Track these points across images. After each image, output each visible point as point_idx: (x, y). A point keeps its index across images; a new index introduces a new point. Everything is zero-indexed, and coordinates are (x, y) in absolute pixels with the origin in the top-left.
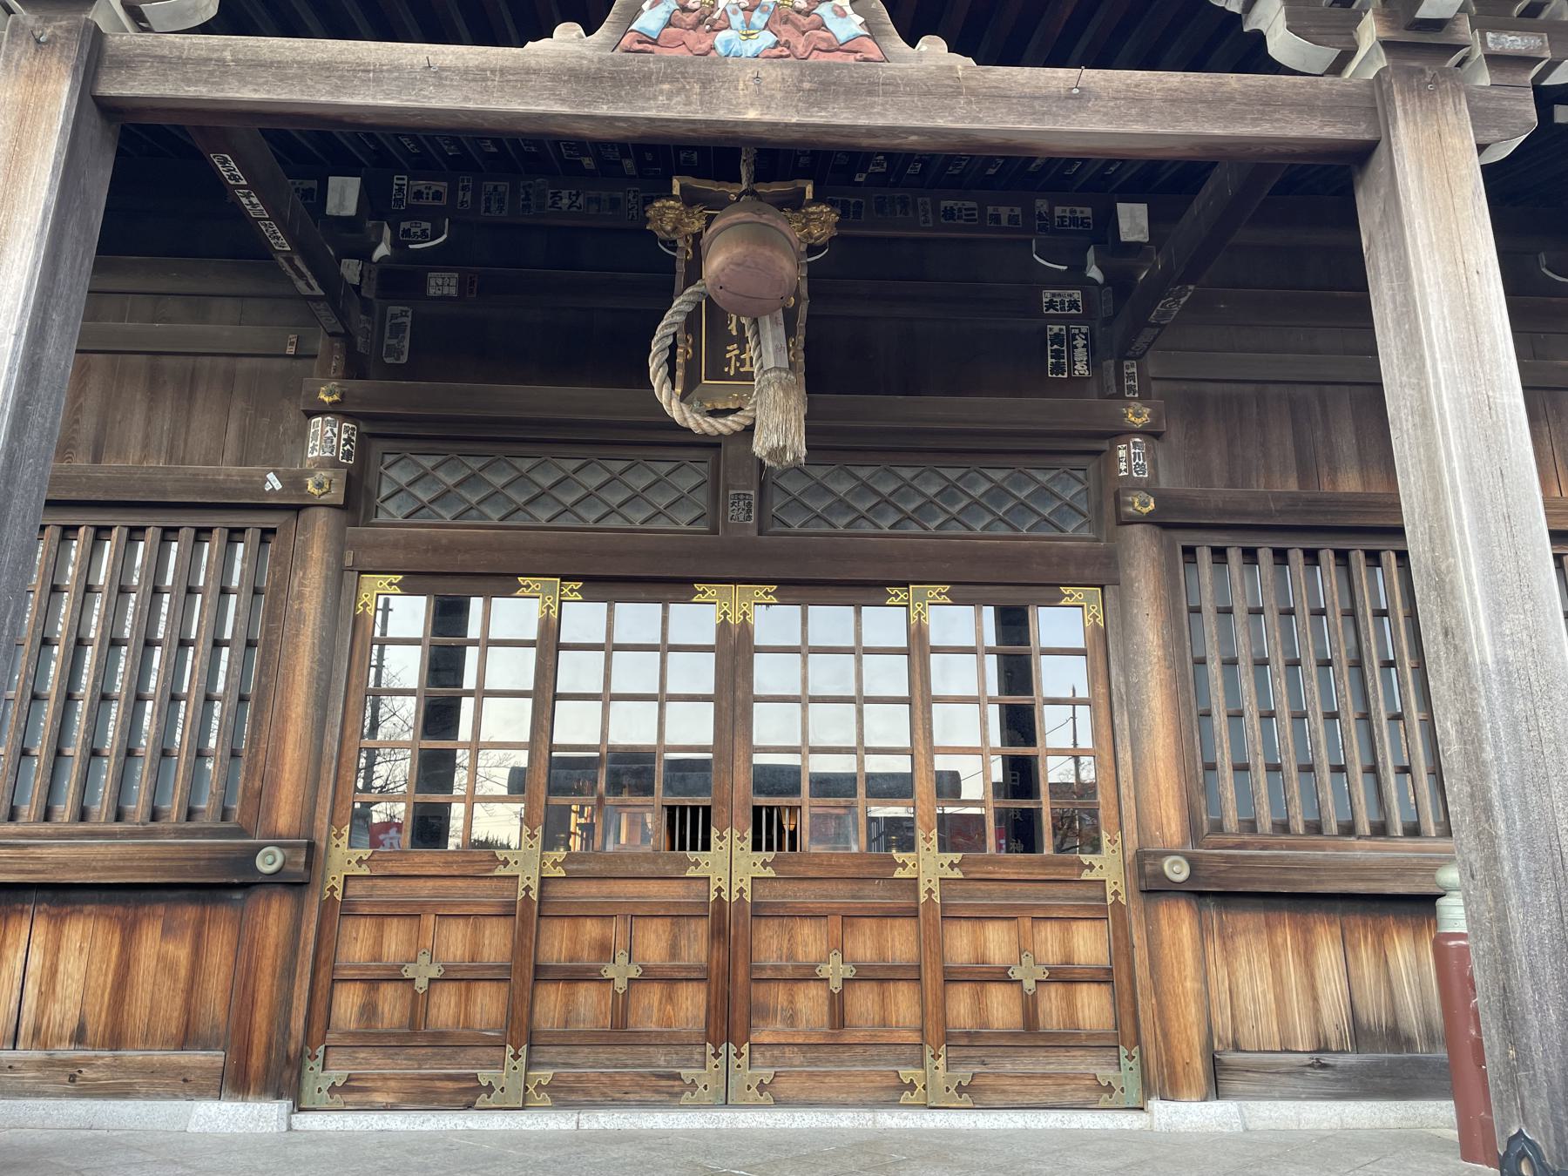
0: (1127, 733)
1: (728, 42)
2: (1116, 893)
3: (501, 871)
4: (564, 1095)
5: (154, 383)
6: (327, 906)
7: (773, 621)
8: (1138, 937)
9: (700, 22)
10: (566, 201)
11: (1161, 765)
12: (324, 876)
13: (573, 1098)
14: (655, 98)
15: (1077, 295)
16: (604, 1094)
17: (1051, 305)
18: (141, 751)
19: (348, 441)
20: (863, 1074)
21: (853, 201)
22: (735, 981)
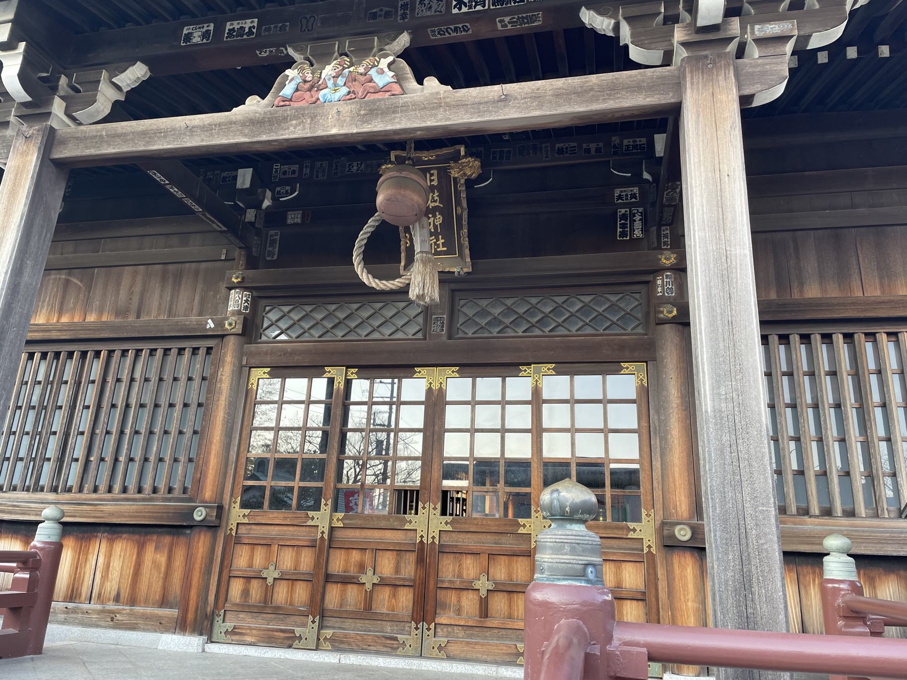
0: (658, 450)
1: (324, 95)
2: (649, 547)
3: (310, 523)
4: (339, 645)
5: (164, 278)
6: (228, 538)
7: (457, 387)
8: (661, 572)
9: (312, 87)
10: (355, 168)
11: (677, 469)
12: (227, 523)
13: (342, 646)
14: (288, 128)
15: (636, 190)
16: (358, 645)
17: (620, 197)
18: (836, 444)
19: (246, 301)
20: (496, 645)
21: (506, 150)
22: (428, 589)
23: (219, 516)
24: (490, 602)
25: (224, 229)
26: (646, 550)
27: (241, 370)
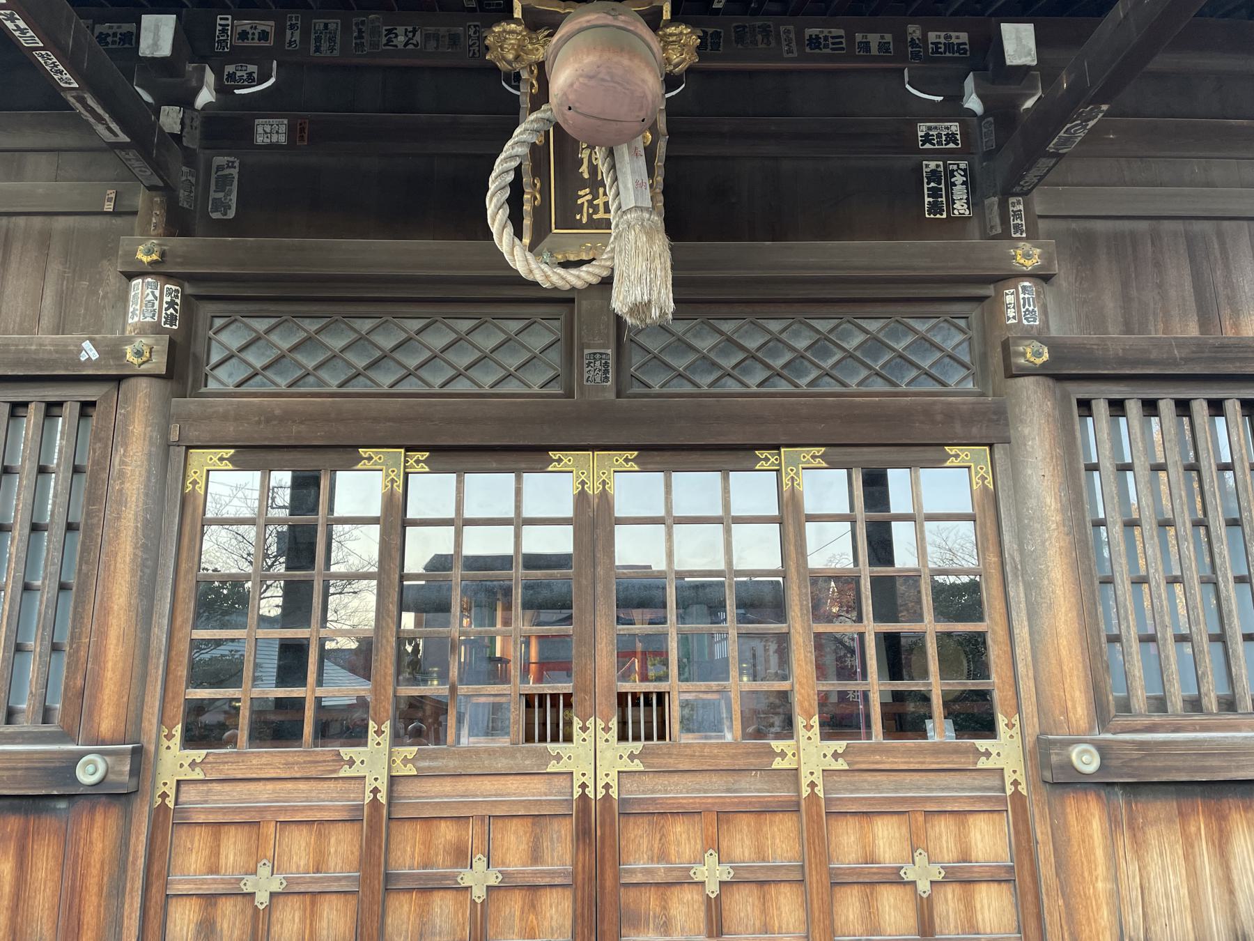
0: (1023, 606)
3: (345, 772)
8: (1041, 831)
10: (401, 39)
15: (955, 127)
17: (927, 139)
19: (172, 304)
23: (136, 772)
24: (726, 906)
25: (123, 138)
26: (1009, 790)
27: (168, 451)
